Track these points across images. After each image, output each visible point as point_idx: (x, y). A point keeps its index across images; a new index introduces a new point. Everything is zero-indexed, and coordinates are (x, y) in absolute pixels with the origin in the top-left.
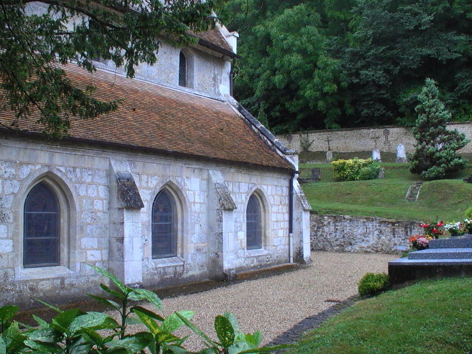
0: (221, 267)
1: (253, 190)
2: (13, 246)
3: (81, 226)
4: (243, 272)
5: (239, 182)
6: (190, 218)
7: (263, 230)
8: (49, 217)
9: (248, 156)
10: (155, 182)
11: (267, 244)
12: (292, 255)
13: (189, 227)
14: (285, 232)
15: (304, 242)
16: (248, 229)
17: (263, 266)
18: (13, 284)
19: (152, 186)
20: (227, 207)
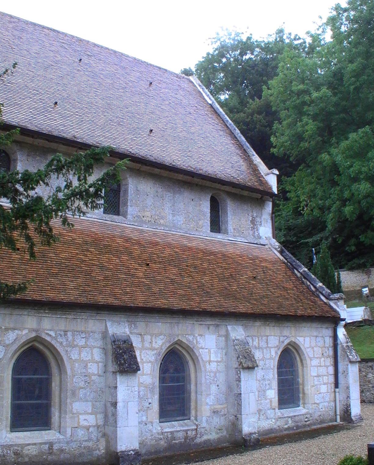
0: (241, 431)
1: (286, 342)
3: (72, 391)
4: (273, 435)
5: (267, 336)
6: (204, 379)
7: (301, 387)
8: (40, 381)
9: (281, 306)
11: (306, 401)
12: (338, 413)
13: (204, 388)
14: (329, 387)
15: (352, 398)
16: (279, 386)
17: (301, 427)
19: (157, 346)
20: (245, 365)
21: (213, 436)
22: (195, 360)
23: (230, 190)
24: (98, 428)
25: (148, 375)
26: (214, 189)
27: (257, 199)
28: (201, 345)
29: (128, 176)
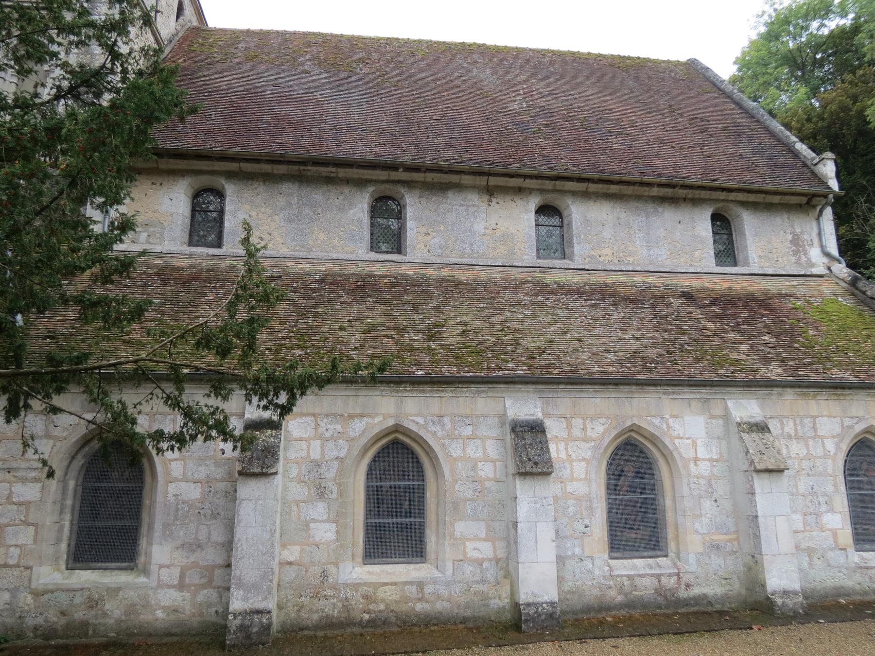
0: (763, 586)
2: (337, 532)
3: (453, 503)
8: (411, 490)
10: (600, 429)
18: (334, 587)
21: (713, 589)
22: (668, 456)
23: (745, 199)
24: (497, 563)
25: (580, 480)
26: (717, 201)
27: (800, 205)
28: (676, 433)
29: (570, 203)
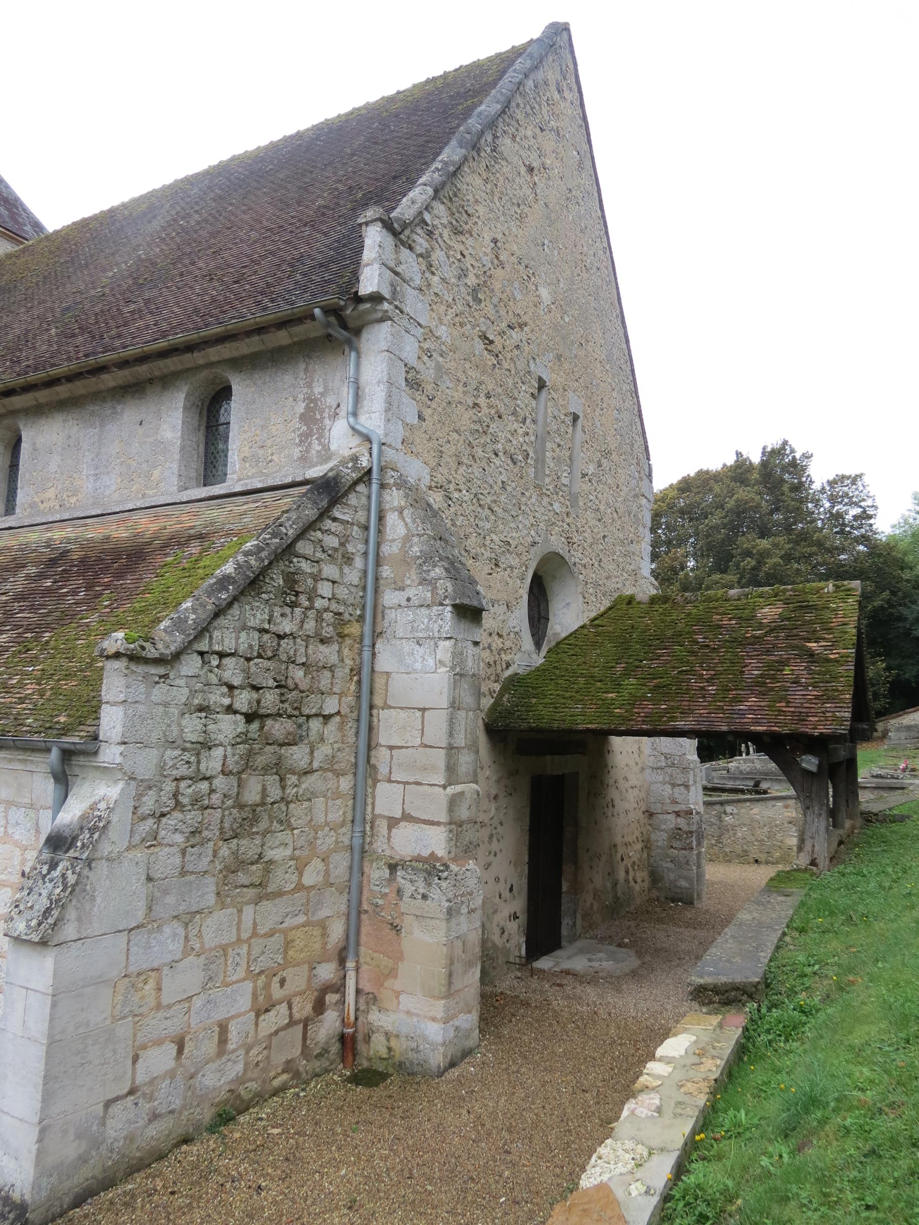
26: (197, 369)
